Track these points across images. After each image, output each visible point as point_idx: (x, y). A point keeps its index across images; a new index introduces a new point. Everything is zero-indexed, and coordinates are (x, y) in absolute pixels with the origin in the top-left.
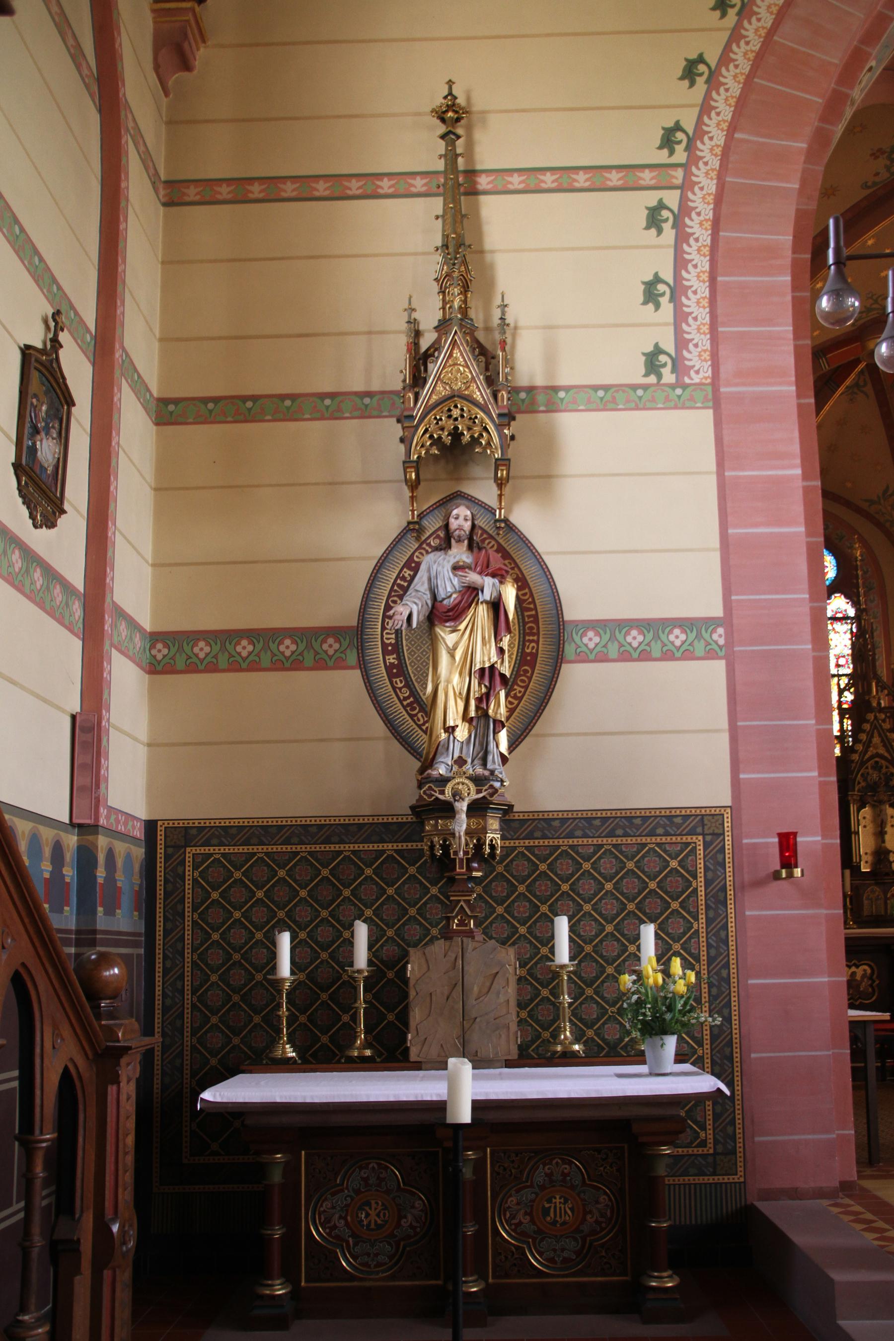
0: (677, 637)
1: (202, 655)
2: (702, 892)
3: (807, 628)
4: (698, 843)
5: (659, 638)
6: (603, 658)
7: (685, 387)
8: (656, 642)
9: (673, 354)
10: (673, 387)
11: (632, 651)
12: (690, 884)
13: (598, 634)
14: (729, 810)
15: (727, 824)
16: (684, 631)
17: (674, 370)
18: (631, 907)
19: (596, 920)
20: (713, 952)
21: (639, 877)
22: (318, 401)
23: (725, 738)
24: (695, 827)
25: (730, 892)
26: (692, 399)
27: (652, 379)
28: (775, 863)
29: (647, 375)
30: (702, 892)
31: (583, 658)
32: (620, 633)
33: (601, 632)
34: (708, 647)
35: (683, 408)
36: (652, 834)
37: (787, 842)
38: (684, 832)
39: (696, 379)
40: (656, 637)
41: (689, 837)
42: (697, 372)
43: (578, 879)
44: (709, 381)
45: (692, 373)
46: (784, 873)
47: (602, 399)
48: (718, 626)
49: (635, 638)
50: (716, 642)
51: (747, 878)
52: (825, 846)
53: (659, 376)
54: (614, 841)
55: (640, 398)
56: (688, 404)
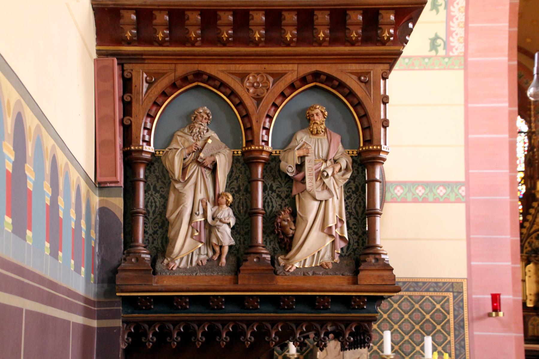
0: (441, 191)
2: (452, 322)
3: (507, 188)
4: (450, 296)
5: (411, 191)
6: (404, 201)
7: (450, 57)
9: (445, 39)
10: (444, 57)
12: (446, 317)
13: (402, 188)
14: (466, 280)
15: (465, 288)
16: (445, 188)
17: (445, 48)
18: (417, 327)
19: (400, 333)
20: (458, 352)
21: (421, 312)
23: (464, 244)
24: (449, 288)
25: (466, 323)
26: (453, 64)
27: (433, 53)
28: (489, 309)
29: (431, 50)
30: (452, 322)
31: (394, 201)
32: (413, 188)
33: (404, 187)
35: (449, 69)
36: (427, 291)
37: (495, 299)
38: (444, 291)
39: (456, 53)
40: (431, 191)
41: (446, 293)
42: (457, 49)
43: (392, 312)
44: (462, 54)
45: (454, 50)
46: (494, 314)
47: (407, 64)
48: (462, 186)
49: (420, 191)
50: (461, 194)
51: (475, 315)
52: (515, 301)
53: (437, 51)
54: (431, 294)
55: (427, 63)
56: (451, 67)
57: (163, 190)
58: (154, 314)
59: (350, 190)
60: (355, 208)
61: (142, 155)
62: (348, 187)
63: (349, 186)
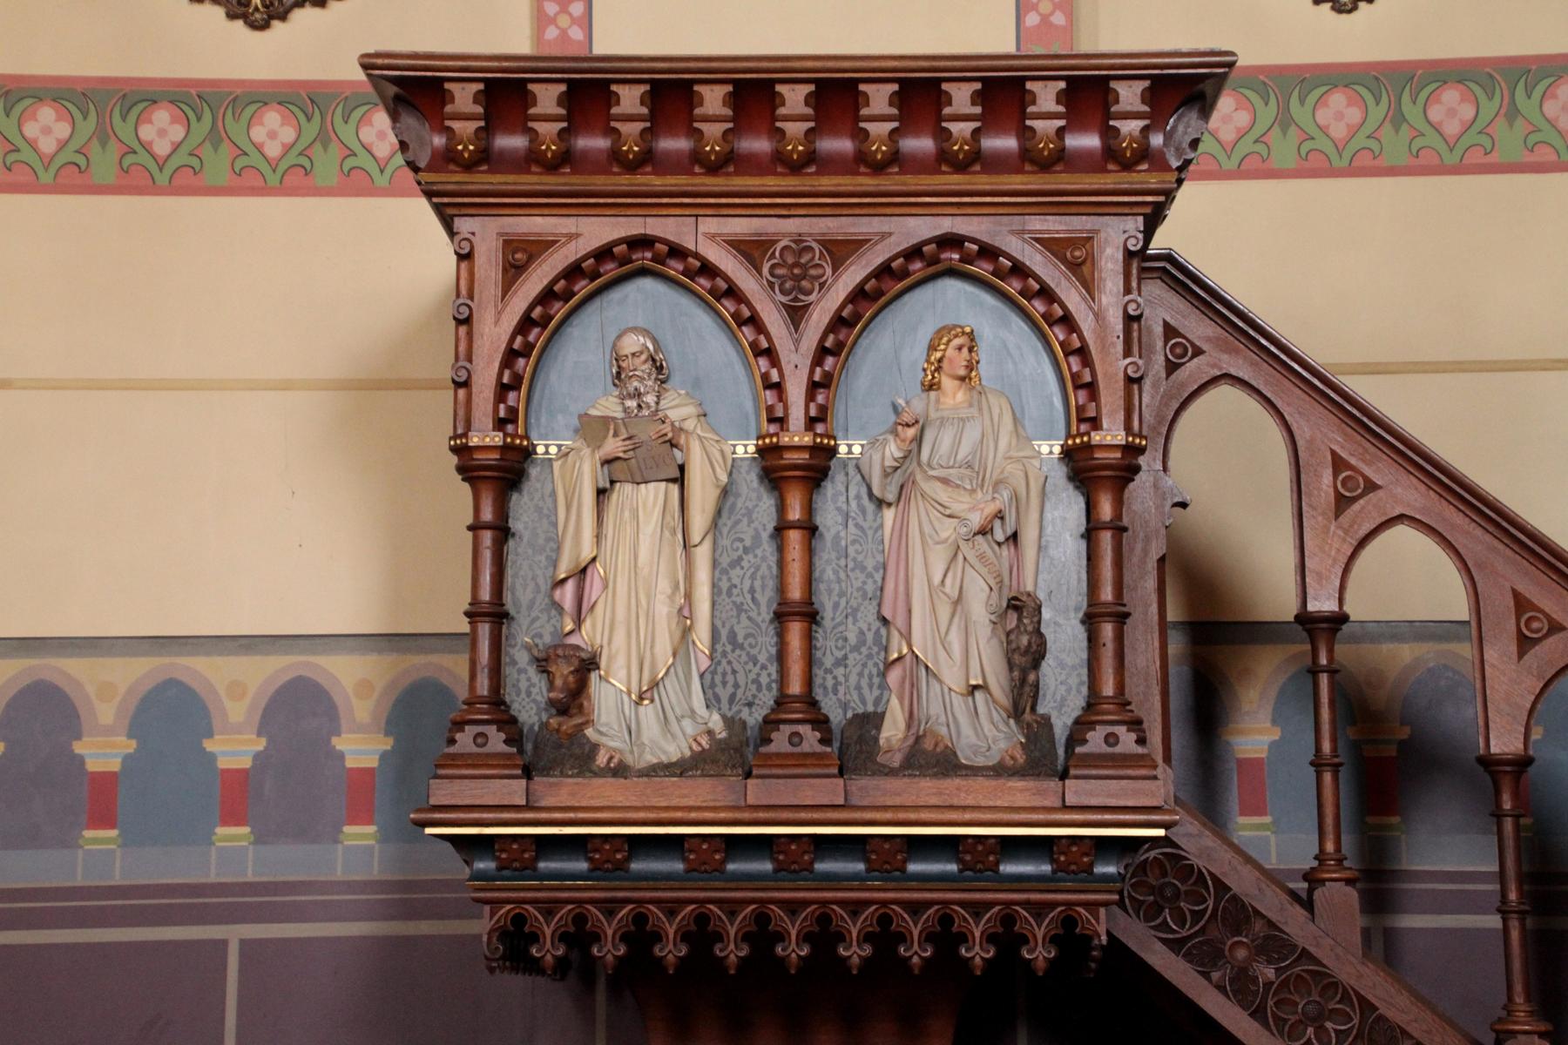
1: (162, 148)
8: (104, 144)
11: (375, 171)
57: (860, 549)
58: (201, 928)
59: (738, 544)
60: (752, 591)
61: (782, 458)
62: (734, 537)
63: (738, 535)
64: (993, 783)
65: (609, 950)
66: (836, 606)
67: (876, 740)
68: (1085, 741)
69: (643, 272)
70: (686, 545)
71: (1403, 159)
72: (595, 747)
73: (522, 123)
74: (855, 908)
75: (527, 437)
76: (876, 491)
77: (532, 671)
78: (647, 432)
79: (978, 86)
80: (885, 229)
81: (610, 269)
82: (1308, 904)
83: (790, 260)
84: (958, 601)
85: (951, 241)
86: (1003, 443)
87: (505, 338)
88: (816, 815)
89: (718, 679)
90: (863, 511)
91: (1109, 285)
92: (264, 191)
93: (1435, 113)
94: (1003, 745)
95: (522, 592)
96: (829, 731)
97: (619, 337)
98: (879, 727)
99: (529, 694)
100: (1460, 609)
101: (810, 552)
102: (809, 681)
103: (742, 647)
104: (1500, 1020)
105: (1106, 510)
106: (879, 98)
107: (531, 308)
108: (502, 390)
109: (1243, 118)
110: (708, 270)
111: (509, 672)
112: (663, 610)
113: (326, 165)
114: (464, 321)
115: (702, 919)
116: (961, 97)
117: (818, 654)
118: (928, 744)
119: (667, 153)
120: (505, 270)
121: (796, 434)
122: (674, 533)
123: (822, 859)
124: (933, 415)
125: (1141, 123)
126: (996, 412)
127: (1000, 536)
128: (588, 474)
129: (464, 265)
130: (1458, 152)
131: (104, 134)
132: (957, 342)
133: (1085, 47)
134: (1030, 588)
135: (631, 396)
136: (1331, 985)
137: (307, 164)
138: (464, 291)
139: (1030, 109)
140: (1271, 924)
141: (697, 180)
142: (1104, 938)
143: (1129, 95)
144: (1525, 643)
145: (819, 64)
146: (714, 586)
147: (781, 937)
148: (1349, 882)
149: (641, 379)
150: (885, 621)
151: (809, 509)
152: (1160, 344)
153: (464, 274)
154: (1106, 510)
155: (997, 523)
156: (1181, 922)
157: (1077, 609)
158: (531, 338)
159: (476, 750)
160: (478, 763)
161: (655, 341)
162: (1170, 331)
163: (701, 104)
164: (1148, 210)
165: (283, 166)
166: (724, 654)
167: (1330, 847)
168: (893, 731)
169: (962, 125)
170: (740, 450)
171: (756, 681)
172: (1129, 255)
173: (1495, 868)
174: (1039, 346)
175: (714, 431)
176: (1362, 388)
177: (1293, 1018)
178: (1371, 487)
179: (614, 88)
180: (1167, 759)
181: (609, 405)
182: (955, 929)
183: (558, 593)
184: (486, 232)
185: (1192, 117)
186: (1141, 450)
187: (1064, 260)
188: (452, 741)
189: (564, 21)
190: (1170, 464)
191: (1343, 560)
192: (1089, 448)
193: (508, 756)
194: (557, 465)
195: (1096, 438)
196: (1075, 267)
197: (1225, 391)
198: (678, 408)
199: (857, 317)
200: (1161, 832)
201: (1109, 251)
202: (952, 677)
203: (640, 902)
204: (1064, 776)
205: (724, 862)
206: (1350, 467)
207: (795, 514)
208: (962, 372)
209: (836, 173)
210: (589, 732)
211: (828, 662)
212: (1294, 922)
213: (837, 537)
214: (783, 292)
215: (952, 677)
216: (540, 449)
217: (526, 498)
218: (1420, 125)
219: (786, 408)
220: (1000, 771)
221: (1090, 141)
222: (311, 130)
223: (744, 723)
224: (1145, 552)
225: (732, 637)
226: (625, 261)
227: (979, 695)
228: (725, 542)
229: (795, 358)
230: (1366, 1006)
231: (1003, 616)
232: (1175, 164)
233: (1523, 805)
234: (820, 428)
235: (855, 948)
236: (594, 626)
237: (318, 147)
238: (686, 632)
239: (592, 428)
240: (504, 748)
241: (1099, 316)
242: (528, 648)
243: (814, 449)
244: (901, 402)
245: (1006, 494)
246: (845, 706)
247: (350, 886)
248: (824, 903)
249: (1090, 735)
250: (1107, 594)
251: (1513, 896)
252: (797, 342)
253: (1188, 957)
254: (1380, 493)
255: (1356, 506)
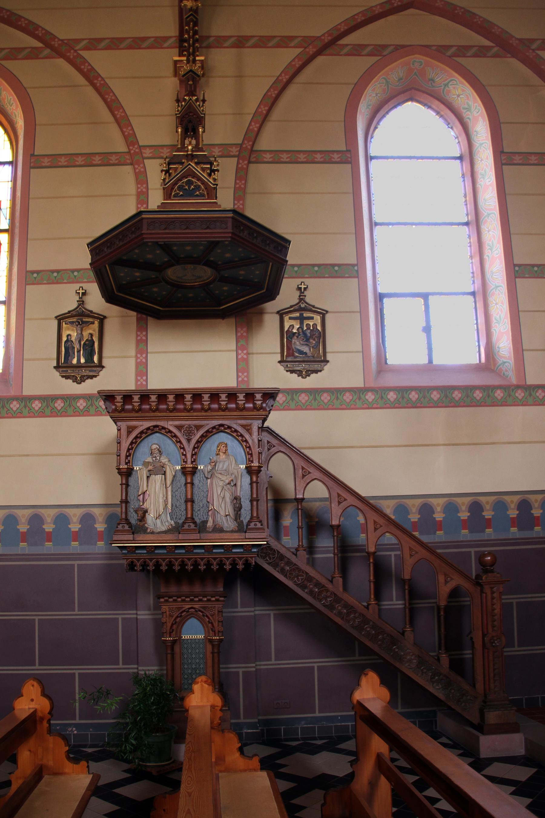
1: (59, 408)
5: (294, 399)
22: (50, 273)
34: (535, 400)
60: (180, 496)
64: (231, 534)
65: (151, 568)
66: (198, 499)
67: (206, 526)
68: (250, 525)
69: (157, 432)
70: (166, 488)
71: (316, 407)
72: (147, 528)
73: (131, 403)
74: (202, 559)
75: (132, 466)
76: (206, 476)
77: (134, 513)
78: (158, 465)
79: (227, 395)
80: (208, 423)
81: (150, 432)
82: (296, 555)
83: (188, 429)
84: (224, 498)
85: (222, 425)
86: (233, 466)
87: (127, 446)
88: (194, 541)
89: (173, 514)
90: (204, 480)
91: (255, 434)
92: (80, 416)
93: (322, 398)
94: (233, 526)
95: (131, 497)
96: (197, 524)
97: (152, 445)
98: (207, 523)
99: (133, 517)
100: (327, 496)
101: (192, 488)
102: (192, 515)
103: (178, 508)
104: (333, 575)
105: (254, 479)
106: (206, 397)
107: (133, 440)
108: (127, 457)
109: (284, 399)
110: (170, 432)
111: (129, 513)
112: (161, 500)
113: (92, 410)
114: (119, 443)
115: (170, 562)
116: (223, 397)
117: (194, 509)
118: (217, 527)
119: (144, 409)
120: (127, 433)
121: (189, 465)
122: (163, 485)
123: (195, 550)
124: (218, 460)
125: (261, 402)
126: (231, 460)
127: (232, 485)
128: (145, 473)
129: (119, 432)
130: (327, 406)
131: (47, 406)
132: (223, 445)
133: (251, 387)
134: (239, 495)
135: (154, 457)
136: (299, 569)
137: (66, 411)
138: (119, 437)
139: (238, 399)
140: (288, 559)
141: (202, 413)
142: (254, 564)
143: (258, 396)
144: (339, 503)
145: (193, 391)
146: (172, 496)
147: (187, 565)
148: (304, 550)
149: (156, 454)
150: (208, 502)
151: (192, 480)
152: (266, 444)
153: (119, 434)
154: (254, 479)
155: (232, 482)
156: (270, 559)
157: (249, 499)
158: (133, 446)
159: (122, 529)
160: (123, 531)
161: (159, 446)
162: (268, 442)
163: (168, 399)
164: (263, 419)
165: (83, 411)
166: (174, 509)
167: (301, 544)
168: (210, 524)
169: (224, 402)
170: (177, 468)
171: (181, 514)
172: (259, 428)
173: (333, 545)
174: (240, 446)
175: (172, 464)
176: (306, 452)
177: (293, 576)
178: (309, 473)
179: (150, 396)
180: (268, 527)
181: (149, 459)
182: (223, 562)
183: (139, 497)
184: (124, 425)
185: (272, 400)
186: (262, 467)
187: (245, 429)
188: (117, 527)
189: (142, 380)
190: (269, 469)
191: (304, 487)
192: (251, 466)
193: (129, 530)
194: (138, 472)
195: (252, 465)
196: (248, 430)
197: (280, 454)
198: (164, 460)
199: (202, 441)
200: (266, 543)
201: (255, 427)
202: (222, 513)
203: (157, 558)
204: (246, 532)
205: (174, 550)
206: (305, 469)
207: (189, 481)
208: (224, 452)
209: (197, 412)
210: (146, 525)
211: (196, 510)
212: (293, 559)
213: (198, 485)
214: (186, 436)
215: (222, 513)
216: (135, 468)
217: (132, 478)
218: (320, 400)
219: (187, 460)
220: (232, 531)
221: (251, 405)
222: (89, 403)
223: (179, 523)
224: (263, 487)
225: (176, 506)
226: (152, 430)
227: (228, 516)
228: (174, 486)
229: (189, 449)
230: (307, 573)
231: (233, 500)
232: (268, 410)
233: (338, 533)
234: (194, 463)
235: (202, 567)
236: (147, 504)
237: (91, 406)
238: (166, 505)
239: (146, 464)
240: (128, 528)
241: (253, 440)
242: (133, 508)
243: (193, 468)
244: (211, 458)
245: (233, 476)
246: (200, 519)
247: (99, 554)
248: (196, 558)
249: (251, 524)
250: (255, 496)
251: (336, 551)
252: (189, 446)
253: (272, 566)
254: (311, 474)
255: (307, 476)
